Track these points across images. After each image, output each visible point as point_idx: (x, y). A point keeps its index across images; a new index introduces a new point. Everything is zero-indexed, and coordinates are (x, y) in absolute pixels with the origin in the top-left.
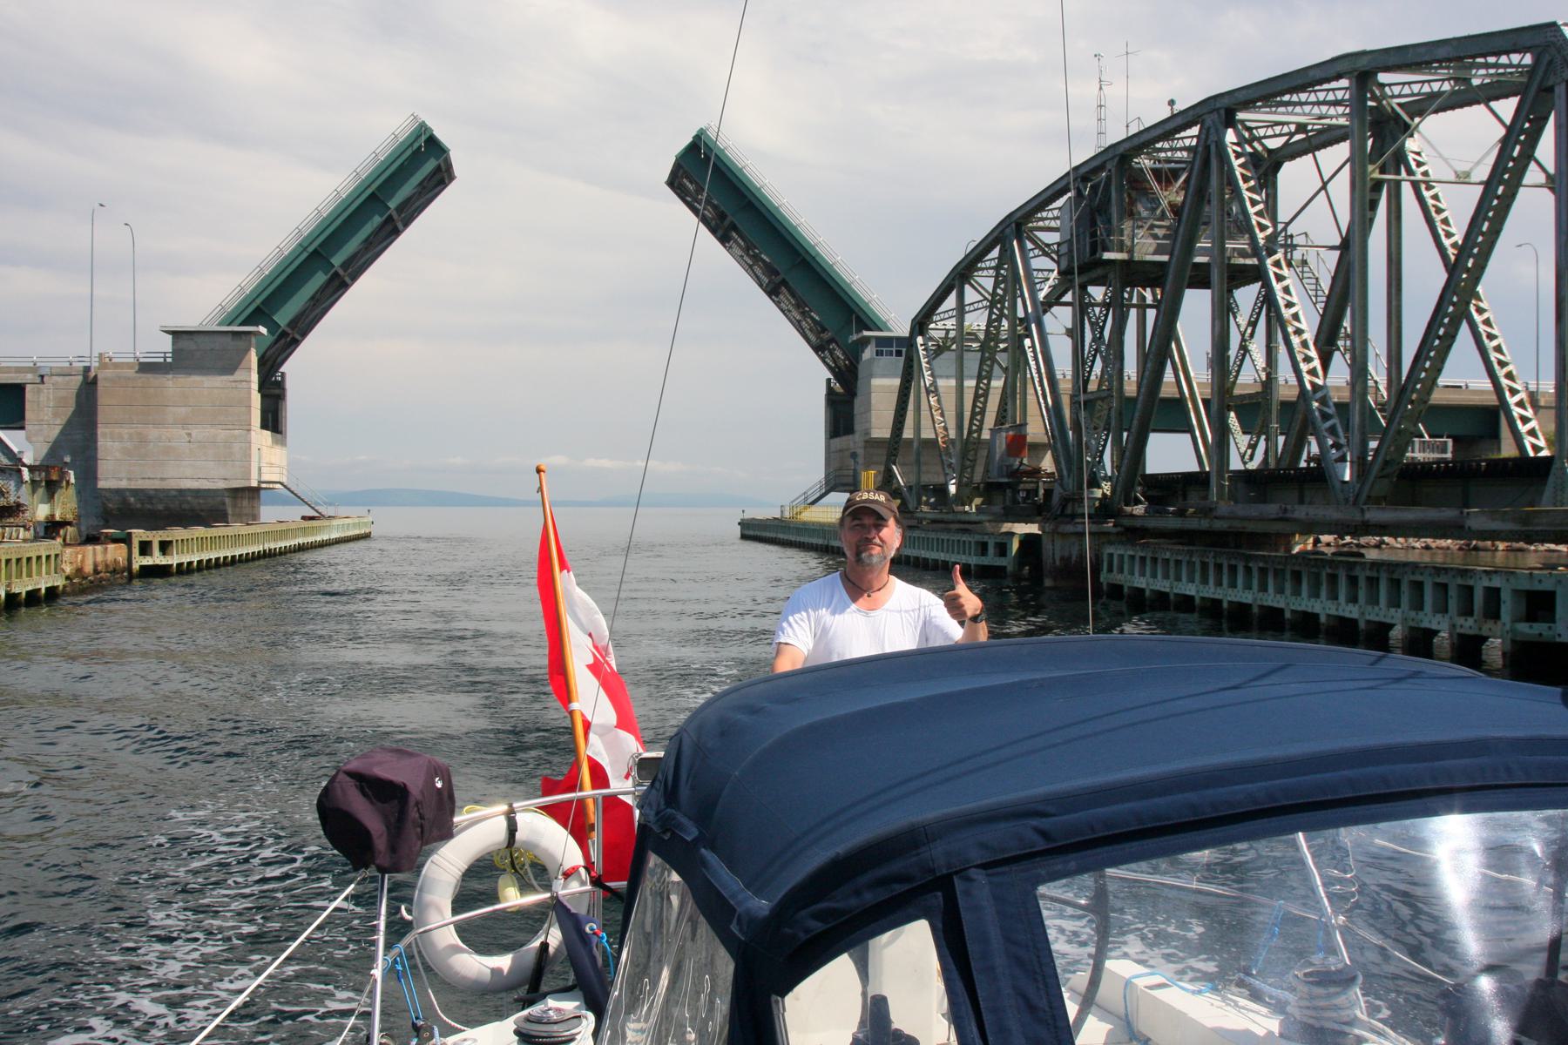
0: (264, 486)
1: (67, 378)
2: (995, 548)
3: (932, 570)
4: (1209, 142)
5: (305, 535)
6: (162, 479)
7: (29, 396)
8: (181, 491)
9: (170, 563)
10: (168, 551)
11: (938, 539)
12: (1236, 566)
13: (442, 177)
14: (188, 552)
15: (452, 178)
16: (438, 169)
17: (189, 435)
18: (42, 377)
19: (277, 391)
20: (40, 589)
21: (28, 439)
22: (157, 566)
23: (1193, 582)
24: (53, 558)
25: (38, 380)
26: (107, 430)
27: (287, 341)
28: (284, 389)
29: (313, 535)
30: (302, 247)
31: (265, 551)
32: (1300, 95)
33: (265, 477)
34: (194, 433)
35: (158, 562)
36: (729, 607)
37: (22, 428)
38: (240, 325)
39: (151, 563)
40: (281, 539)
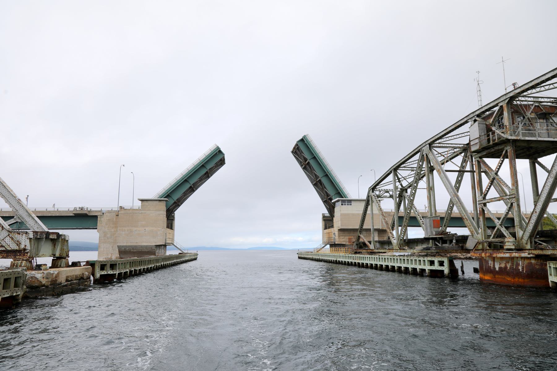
0: (167, 244)
1: (110, 214)
2: (428, 263)
3: (391, 271)
4: (424, 154)
5: (177, 259)
6: (137, 243)
7: (99, 219)
8: (141, 246)
9: (115, 273)
10: (114, 267)
11: (363, 257)
12: (434, 261)
13: (222, 162)
14: (137, 266)
15: (224, 163)
16: (221, 160)
17: (145, 229)
18: (103, 213)
19: (172, 218)
20: (116, 274)
21: (98, 231)
22: (109, 274)
23: (421, 265)
24: (134, 262)
25: (102, 214)
26: (121, 228)
27: (178, 204)
28: (174, 218)
29: (179, 259)
30: (182, 178)
31: (161, 265)
32: (528, 91)
33: (167, 242)
34: (147, 229)
35: (109, 273)
36: (376, 338)
37: (96, 229)
38: (164, 198)
39: (106, 273)
40: (168, 261)
